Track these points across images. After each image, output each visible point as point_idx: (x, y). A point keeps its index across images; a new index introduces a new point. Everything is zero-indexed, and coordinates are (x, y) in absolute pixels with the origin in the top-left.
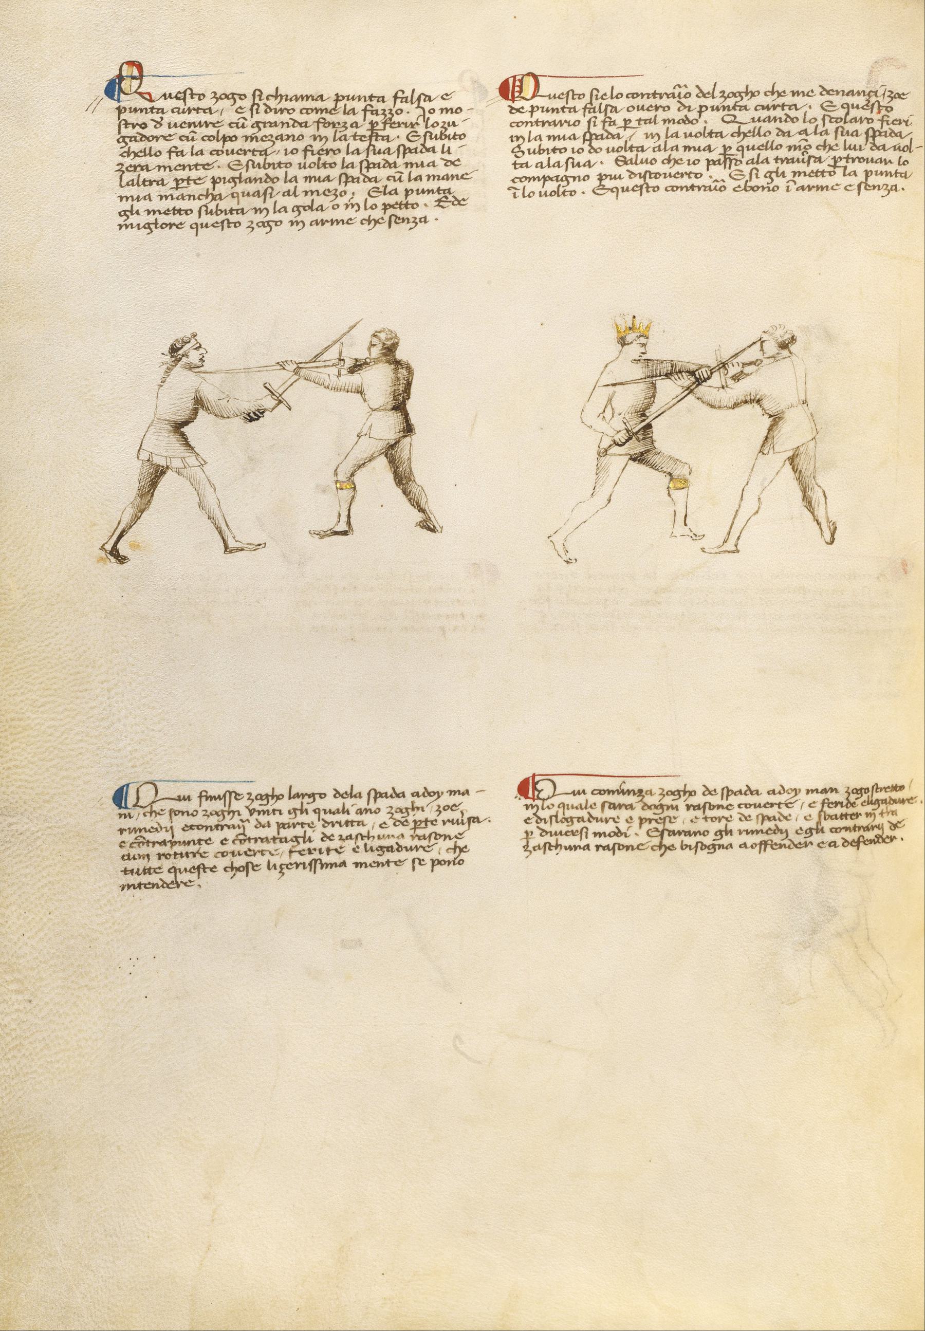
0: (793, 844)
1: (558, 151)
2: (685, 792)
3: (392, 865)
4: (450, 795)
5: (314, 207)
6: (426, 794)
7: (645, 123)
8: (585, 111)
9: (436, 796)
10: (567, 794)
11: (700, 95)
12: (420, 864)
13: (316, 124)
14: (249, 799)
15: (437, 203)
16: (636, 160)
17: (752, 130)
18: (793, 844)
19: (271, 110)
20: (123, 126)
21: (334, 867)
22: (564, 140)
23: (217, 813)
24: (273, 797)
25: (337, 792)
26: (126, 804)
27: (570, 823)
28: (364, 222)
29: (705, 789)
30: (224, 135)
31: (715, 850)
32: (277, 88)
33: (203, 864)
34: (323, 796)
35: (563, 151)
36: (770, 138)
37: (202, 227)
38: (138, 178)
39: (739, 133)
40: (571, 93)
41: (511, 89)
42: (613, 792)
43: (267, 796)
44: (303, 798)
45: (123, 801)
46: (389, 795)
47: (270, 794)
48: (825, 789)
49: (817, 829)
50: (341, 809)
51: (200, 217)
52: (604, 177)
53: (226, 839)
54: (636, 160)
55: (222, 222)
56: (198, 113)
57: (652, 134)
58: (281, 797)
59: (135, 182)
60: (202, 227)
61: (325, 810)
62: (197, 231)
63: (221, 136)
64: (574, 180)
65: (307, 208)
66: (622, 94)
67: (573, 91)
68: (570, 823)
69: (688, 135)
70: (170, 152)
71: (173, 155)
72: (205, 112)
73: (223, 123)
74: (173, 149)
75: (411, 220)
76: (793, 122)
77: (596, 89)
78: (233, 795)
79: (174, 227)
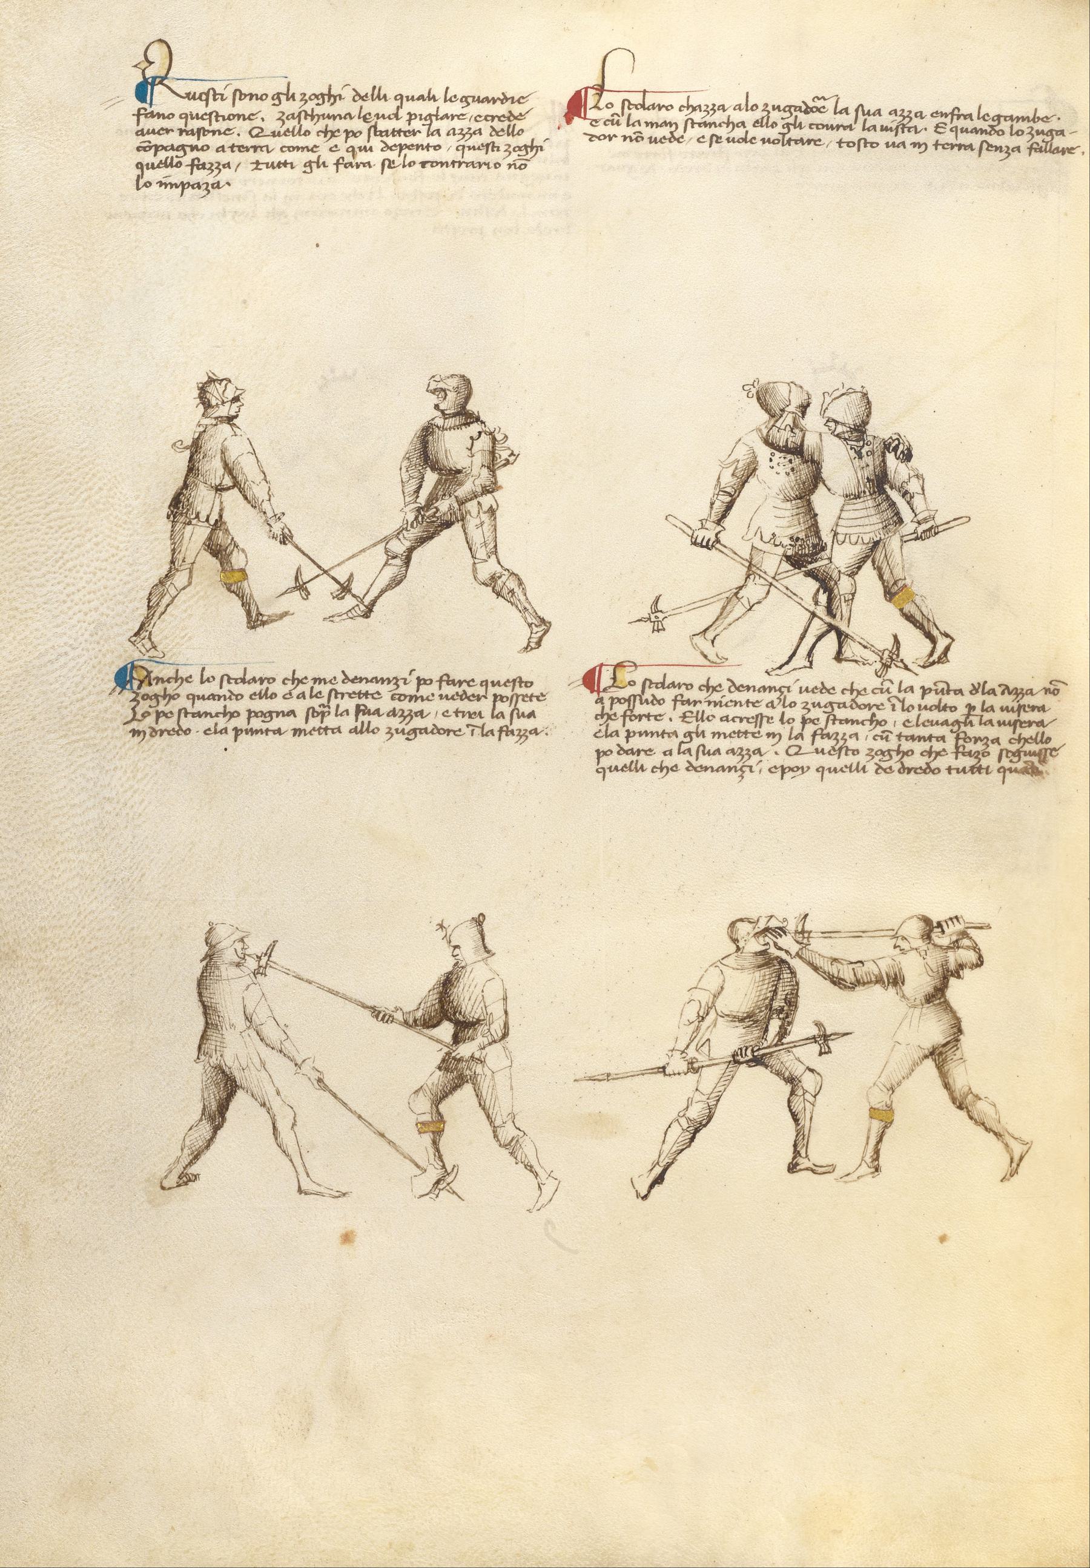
2: (532, 147)
4: (133, 736)
5: (666, 685)
6: (655, 702)
7: (841, 723)
9: (800, 771)
10: (335, 1096)
12: (768, 722)
14: (301, 100)
15: (255, 166)
16: (747, 105)
20: (182, 715)
21: (961, 768)
22: (721, 706)
23: (317, 97)
24: (164, 697)
26: (585, 115)
27: (268, 719)
29: (355, 93)
32: (852, 683)
34: (1031, 692)
35: (875, 145)
37: (408, 100)
38: (747, 101)
42: (494, 101)
43: (323, 95)
44: (638, 755)
46: (429, 730)
47: (326, 91)
49: (287, 94)
50: (426, 95)
52: (632, 734)
54: (747, 105)
56: (649, 720)
58: (609, 753)
60: (408, 100)
61: (407, 97)
65: (639, 107)
66: (267, 95)
68: (268, 719)
76: (660, 704)
79: (451, 734)
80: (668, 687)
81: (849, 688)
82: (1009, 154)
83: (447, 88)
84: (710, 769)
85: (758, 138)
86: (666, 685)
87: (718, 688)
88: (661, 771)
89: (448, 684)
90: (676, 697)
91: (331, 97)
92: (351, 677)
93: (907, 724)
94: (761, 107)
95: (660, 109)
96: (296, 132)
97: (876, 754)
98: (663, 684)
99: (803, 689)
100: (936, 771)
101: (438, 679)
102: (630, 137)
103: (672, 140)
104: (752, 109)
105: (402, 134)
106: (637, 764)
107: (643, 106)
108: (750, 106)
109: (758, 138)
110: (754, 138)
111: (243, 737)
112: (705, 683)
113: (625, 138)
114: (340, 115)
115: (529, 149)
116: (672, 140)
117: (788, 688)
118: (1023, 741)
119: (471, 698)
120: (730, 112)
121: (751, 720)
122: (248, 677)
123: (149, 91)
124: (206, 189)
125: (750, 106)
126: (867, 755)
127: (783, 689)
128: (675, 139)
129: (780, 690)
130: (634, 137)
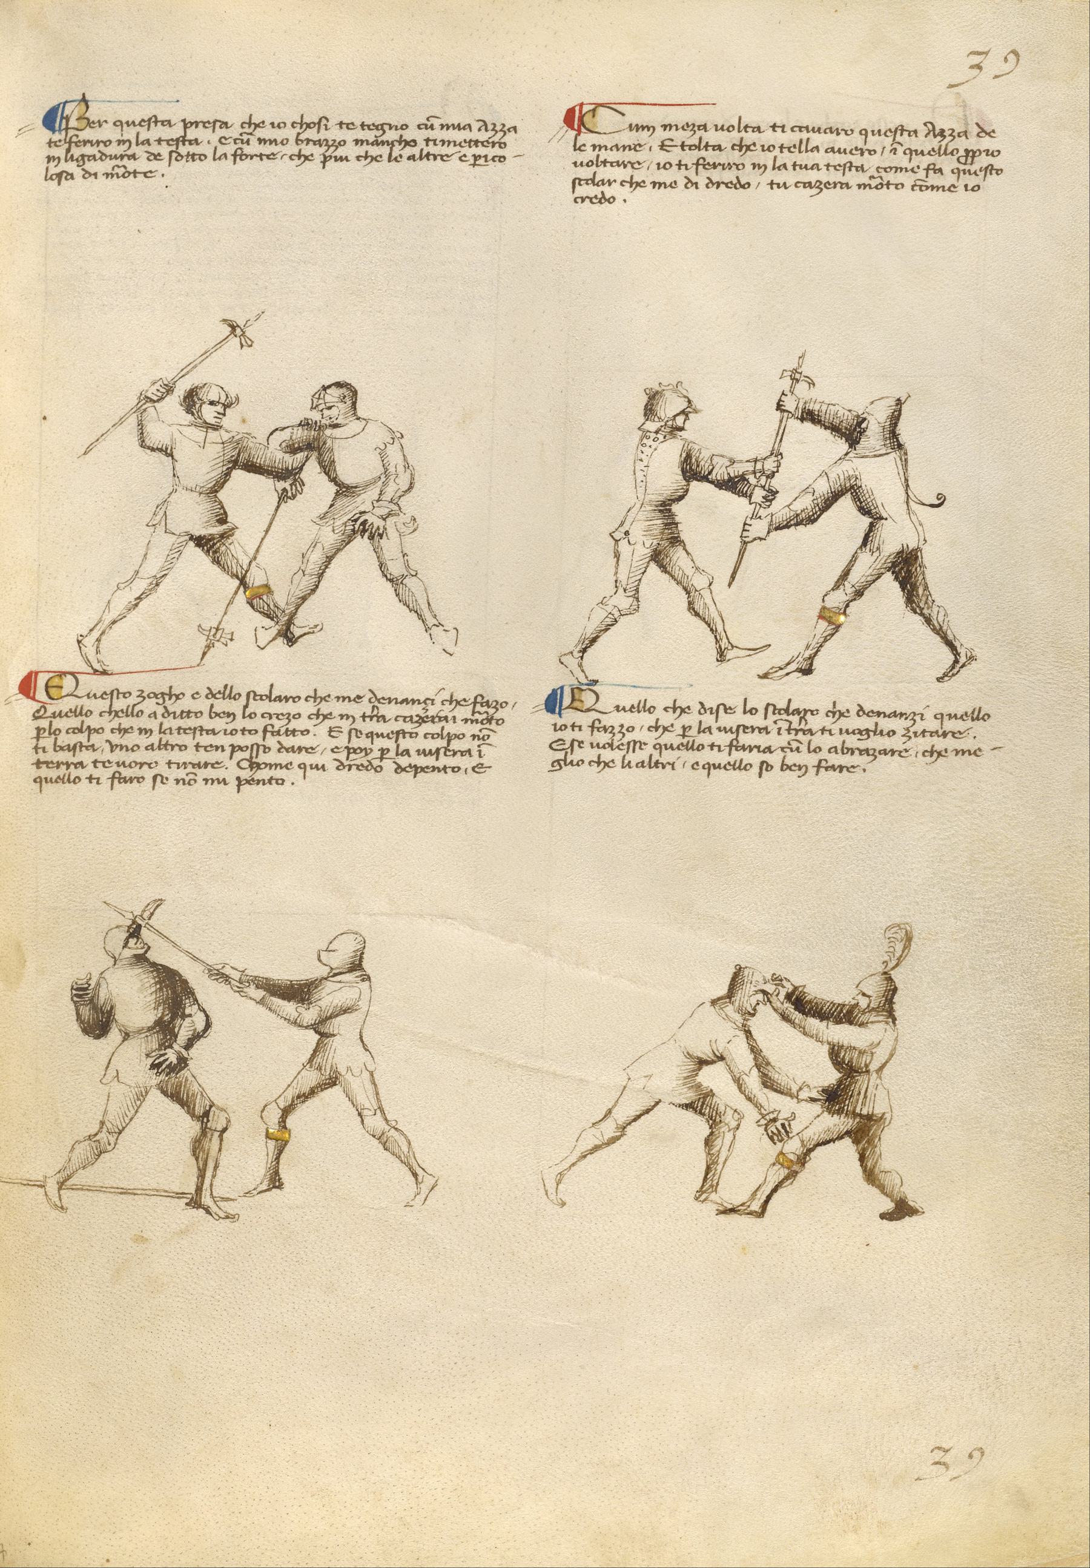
0: (376, 697)
1: (165, 143)
3: (892, 187)
8: (730, 750)
11: (210, 696)
13: (695, 166)
17: (732, 763)
18: (376, 697)
19: (713, 184)
23: (156, 696)
25: (861, 709)
28: (293, 157)
30: (449, 733)
31: (561, 768)
33: (851, 163)
36: (115, 724)
39: (318, 715)
40: (115, 693)
41: (558, 697)
45: (32, 691)
47: (167, 691)
48: (280, 696)
51: (765, 718)
53: (465, 156)
55: (398, 733)
56: (261, 159)
57: (609, 181)
59: (156, 746)
62: (942, 721)
63: (445, 733)
64: (390, 128)
67: (118, 690)
69: (719, 128)
70: (592, 727)
71: (931, 172)
72: (315, 144)
73: (222, 765)
74: (701, 161)
75: (871, 752)
77: (481, 696)
78: (261, 748)
80: (275, 700)
81: (672, 706)
82: (876, 757)
83: (251, 115)
84: (347, 700)
85: (259, 713)
86: (273, 698)
87: (846, 714)
88: (317, 718)
89: (120, 783)
90: (236, 151)
91: (934, 753)
92: (867, 710)
93: (223, 140)
94: (135, 694)
95: (287, 701)
96: (942, 152)
97: (627, 730)
98: (269, 697)
99: (578, 164)
100: (461, 736)
101: (728, 743)
102: (184, 780)
103: (603, 201)
104: (396, 159)
105: (480, 144)
106: (979, 712)
107: (269, 697)
108: (812, 748)
109: (259, 713)
110: (584, 145)
111: (330, 164)
112: (654, 725)
113: (177, 781)
114: (969, 751)
115: (167, 698)
116: (603, 201)
117: (433, 700)
118: (454, 703)
119: (730, 185)
120: (659, 713)
121: (171, 142)
122: (273, 697)
123: (33, 685)
124: (873, 755)
125: (812, 748)
126: (138, 696)
127: (428, 702)
128: (606, 200)
129: (425, 702)
130: (187, 779)
